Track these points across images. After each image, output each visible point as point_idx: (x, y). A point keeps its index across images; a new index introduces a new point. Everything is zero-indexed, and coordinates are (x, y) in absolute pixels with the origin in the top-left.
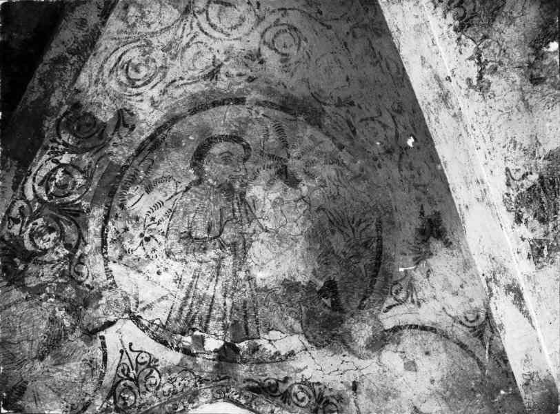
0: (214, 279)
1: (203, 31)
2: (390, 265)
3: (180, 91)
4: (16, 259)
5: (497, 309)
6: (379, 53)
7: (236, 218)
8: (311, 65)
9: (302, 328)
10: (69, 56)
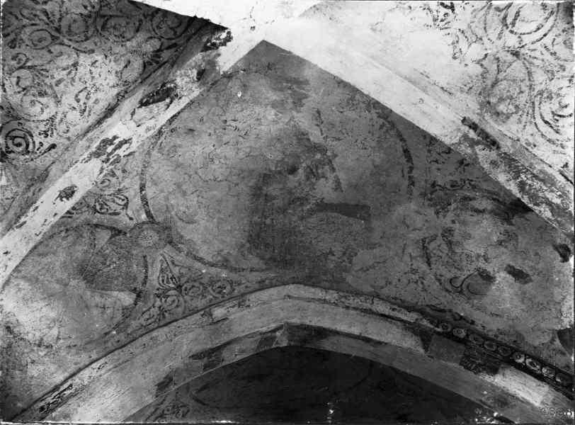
1: (541, 39)
10: (520, 180)
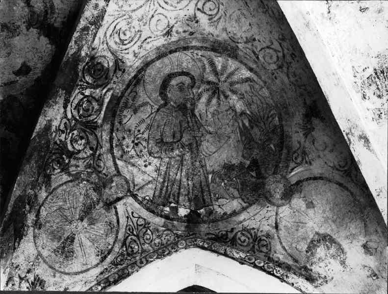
0: (180, 169)
1: (160, 6)
2: (290, 141)
3: (150, 45)
4: (64, 156)
5: (354, 151)
6: (267, 5)
7: (189, 127)
8: (227, 19)
9: (239, 194)
